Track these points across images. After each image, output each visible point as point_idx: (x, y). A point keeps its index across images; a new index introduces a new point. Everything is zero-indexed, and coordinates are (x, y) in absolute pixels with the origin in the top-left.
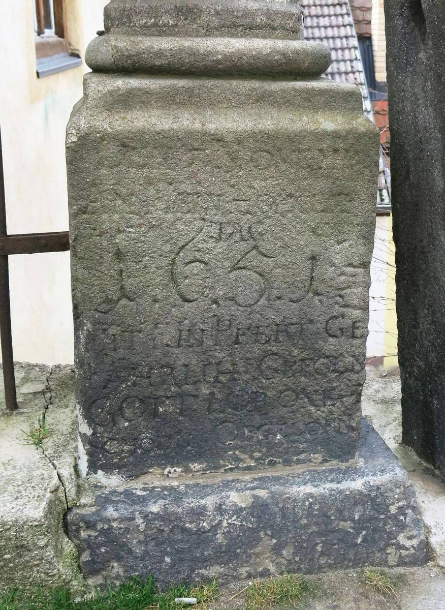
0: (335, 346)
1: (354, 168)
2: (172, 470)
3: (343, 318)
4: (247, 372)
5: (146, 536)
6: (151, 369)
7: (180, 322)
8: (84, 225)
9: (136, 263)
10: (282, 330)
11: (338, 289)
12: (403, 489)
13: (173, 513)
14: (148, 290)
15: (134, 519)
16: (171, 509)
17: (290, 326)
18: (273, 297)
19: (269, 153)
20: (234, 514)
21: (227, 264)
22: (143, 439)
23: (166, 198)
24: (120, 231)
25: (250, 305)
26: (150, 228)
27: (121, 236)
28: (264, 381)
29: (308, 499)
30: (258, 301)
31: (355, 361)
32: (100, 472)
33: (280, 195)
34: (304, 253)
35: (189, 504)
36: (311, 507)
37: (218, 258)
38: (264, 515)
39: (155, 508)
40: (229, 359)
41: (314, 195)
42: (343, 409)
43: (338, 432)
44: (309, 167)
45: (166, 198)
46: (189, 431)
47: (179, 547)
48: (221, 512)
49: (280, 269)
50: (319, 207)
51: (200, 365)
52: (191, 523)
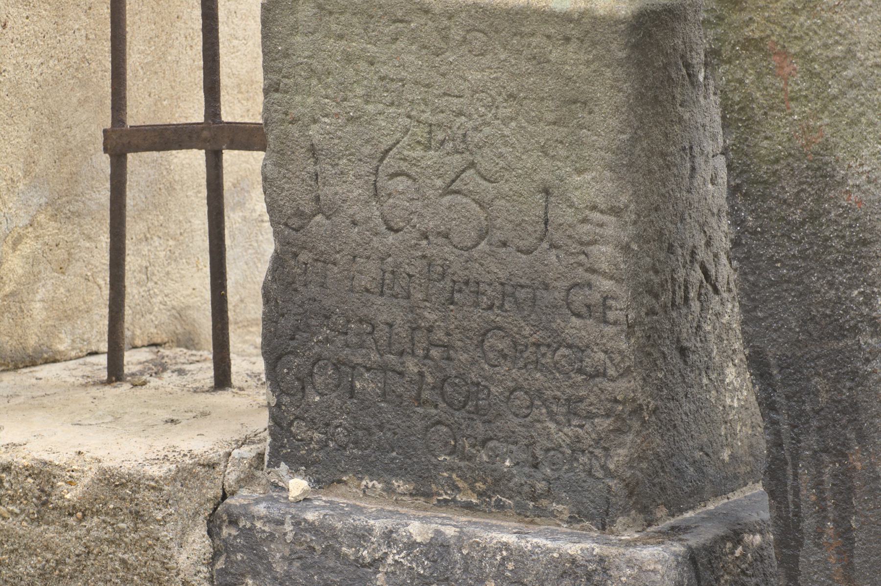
0: (579, 330)
1: (592, 66)
2: (370, 485)
3: (590, 288)
4: (465, 350)
5: (293, 552)
6: (349, 322)
7: (383, 259)
8: (276, 106)
9: (333, 166)
10: (508, 291)
11: (582, 244)
12: (636, 570)
13: (332, 528)
14: (345, 206)
15: (282, 523)
16: (330, 521)
17: (519, 289)
18: (495, 240)
19: (485, 34)
20: (405, 549)
21: (439, 183)
22: (337, 427)
23: (365, 82)
24: (315, 121)
25: (468, 249)
26: (348, 120)
27: (316, 127)
28: (486, 367)
29: (501, 551)
30: (478, 244)
31: (607, 361)
32: (283, 466)
33: (500, 94)
34: (533, 181)
35: (355, 521)
36: (503, 565)
37: (426, 173)
38: (442, 559)
39: (311, 516)
40: (442, 324)
41: (542, 99)
42: (594, 436)
43: (590, 473)
44: (534, 58)
45: (365, 82)
46: (393, 427)
47: (328, 578)
48: (389, 543)
49: (504, 201)
50: (550, 117)
51: (406, 327)
52: (349, 547)
